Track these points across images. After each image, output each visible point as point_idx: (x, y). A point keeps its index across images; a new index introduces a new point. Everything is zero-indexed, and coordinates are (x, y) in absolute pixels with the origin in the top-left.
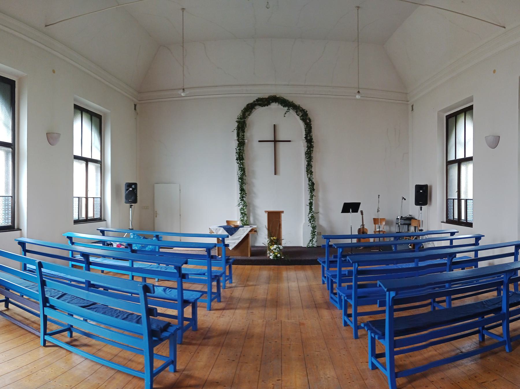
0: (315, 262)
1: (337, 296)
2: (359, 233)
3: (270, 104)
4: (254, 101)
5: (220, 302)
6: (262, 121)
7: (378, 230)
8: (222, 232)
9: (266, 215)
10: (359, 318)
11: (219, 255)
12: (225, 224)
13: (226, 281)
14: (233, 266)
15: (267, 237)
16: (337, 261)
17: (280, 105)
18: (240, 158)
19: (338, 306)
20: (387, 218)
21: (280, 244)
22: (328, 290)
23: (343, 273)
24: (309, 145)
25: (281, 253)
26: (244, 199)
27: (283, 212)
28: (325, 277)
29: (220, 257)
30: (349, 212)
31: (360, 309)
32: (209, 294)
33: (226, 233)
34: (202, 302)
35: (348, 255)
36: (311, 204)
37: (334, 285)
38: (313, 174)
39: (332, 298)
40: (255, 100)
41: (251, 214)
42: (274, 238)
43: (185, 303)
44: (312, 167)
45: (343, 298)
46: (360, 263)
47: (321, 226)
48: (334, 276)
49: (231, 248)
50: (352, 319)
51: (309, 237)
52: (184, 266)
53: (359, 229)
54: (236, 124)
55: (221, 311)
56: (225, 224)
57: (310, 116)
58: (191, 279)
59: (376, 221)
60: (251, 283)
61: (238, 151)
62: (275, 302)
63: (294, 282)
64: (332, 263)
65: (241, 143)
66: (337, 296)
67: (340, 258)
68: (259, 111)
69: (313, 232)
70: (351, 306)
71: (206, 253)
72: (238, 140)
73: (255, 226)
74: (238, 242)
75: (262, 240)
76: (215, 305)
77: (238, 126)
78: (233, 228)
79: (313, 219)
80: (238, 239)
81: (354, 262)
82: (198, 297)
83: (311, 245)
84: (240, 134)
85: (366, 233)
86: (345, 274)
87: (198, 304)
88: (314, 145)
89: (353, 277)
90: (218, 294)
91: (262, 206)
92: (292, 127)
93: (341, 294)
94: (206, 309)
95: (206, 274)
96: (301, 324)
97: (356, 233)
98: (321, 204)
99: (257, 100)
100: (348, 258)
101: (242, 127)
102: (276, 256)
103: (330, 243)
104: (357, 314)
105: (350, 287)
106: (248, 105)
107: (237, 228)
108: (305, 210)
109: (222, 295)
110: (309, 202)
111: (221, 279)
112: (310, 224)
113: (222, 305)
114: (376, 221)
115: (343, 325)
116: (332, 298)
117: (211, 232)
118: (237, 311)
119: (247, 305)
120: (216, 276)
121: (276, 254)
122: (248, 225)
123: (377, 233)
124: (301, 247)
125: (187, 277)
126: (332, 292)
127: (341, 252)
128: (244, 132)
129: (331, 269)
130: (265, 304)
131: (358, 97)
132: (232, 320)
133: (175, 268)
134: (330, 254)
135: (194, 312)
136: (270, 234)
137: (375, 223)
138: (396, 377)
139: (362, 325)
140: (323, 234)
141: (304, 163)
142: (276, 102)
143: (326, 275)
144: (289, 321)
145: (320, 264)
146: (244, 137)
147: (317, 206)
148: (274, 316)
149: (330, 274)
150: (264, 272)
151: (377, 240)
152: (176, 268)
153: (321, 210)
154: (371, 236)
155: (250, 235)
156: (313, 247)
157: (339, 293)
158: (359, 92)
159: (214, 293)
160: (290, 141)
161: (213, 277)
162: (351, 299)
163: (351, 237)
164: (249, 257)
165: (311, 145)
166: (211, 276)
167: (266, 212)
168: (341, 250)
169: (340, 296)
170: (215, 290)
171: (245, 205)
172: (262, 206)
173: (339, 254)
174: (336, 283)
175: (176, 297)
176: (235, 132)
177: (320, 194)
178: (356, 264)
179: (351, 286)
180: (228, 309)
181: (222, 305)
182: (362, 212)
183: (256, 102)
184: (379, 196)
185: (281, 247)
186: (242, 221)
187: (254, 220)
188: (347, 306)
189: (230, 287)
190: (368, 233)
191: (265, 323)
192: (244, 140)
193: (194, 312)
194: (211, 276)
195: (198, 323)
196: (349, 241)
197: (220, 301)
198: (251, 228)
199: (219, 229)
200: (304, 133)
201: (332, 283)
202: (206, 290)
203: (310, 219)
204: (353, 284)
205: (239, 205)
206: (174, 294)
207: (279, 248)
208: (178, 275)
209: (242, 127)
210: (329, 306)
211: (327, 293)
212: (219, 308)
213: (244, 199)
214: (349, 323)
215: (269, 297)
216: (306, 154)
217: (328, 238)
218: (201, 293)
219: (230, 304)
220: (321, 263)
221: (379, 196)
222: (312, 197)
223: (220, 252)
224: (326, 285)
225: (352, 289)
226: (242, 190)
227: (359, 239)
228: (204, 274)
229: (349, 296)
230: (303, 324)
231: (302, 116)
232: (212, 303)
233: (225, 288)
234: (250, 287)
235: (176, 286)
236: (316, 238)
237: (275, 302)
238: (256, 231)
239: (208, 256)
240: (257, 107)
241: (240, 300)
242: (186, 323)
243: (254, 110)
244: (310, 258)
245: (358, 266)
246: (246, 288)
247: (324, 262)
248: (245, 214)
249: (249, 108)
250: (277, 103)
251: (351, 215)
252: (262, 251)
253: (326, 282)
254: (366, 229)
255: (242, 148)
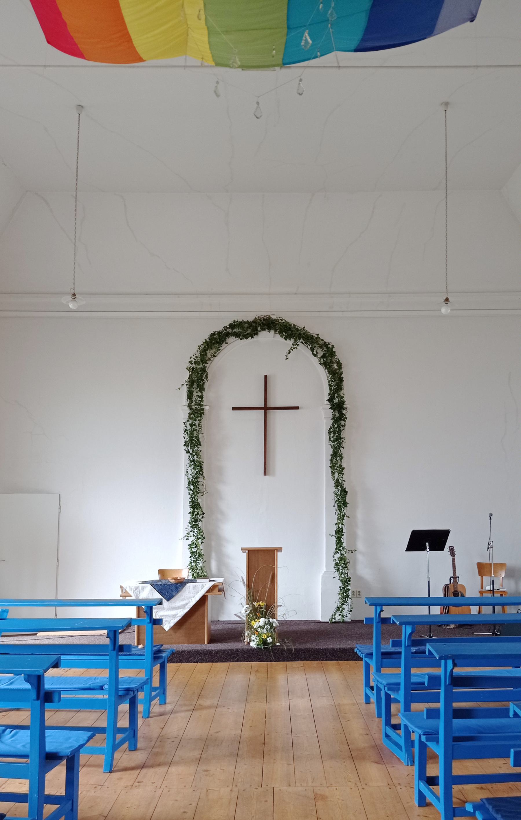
0: (348, 655)
1: (402, 732)
2: (445, 595)
3: (256, 334)
4: (226, 328)
5: (136, 749)
6: (239, 369)
7: (488, 588)
8: (150, 594)
9: (244, 556)
10: (456, 788)
11: (138, 644)
12: (156, 577)
13: (152, 699)
14: (170, 667)
15: (244, 601)
16: (400, 653)
17: (278, 336)
18: (193, 442)
19: (403, 755)
20: (510, 562)
21: (273, 616)
22: (380, 716)
23: (414, 680)
24: (338, 415)
25: (275, 635)
26: (200, 524)
27: (280, 549)
28: (372, 688)
29: (140, 646)
30: (423, 549)
31: (460, 768)
32: (110, 731)
33: (157, 596)
34: (93, 752)
35: (430, 641)
36: (339, 533)
37: (394, 707)
38: (345, 471)
39: (387, 736)
40: (227, 324)
41: (213, 555)
42: (261, 603)
43: (51, 759)
44: (342, 458)
45: (415, 737)
46: (457, 660)
47: (360, 579)
48: (394, 687)
49: (167, 626)
50: (440, 789)
51: (335, 600)
52: (52, 672)
53: (447, 585)
54: (187, 374)
55: (136, 772)
56: (156, 577)
57: (340, 355)
58: (67, 700)
59: (483, 569)
60: (207, 702)
61: (189, 427)
62: (260, 746)
63: (303, 697)
64: (388, 657)
65: (196, 413)
66: (402, 732)
67: (407, 647)
68: (234, 346)
69: (344, 594)
70: (435, 757)
71: (107, 641)
72: (190, 407)
73: (220, 580)
74: (181, 613)
75: (235, 608)
76: (124, 757)
77: (190, 377)
78: (172, 584)
79: (342, 564)
80: (184, 606)
81: (446, 658)
82: (82, 742)
83: (338, 618)
84: (195, 394)
85: (463, 595)
86: (423, 684)
87: (83, 758)
88: (348, 413)
89: (442, 691)
90: (132, 730)
91: (237, 538)
92: (302, 378)
93: (411, 727)
94: (102, 770)
95: (106, 687)
96: (317, 797)
97: (438, 593)
98: (360, 533)
99: (231, 325)
100: (428, 647)
101: (197, 379)
102: (265, 642)
103: (383, 615)
104: (452, 780)
105: (433, 714)
106: (213, 335)
107: (181, 584)
108: (326, 545)
109: (140, 734)
110: (335, 528)
111: (141, 696)
112: (337, 574)
113: (139, 757)
114: (483, 569)
115: (416, 803)
116: (387, 736)
117: (125, 593)
118: (173, 769)
119: (197, 753)
120: (128, 690)
121: (264, 637)
122: (205, 577)
123: (485, 595)
124: (319, 622)
125: (56, 697)
126: (388, 722)
127: (410, 634)
128: (202, 389)
129: (384, 671)
130: (237, 750)
131: (445, 310)
132: (159, 792)
133: (27, 681)
134: (383, 636)
135: (71, 782)
136: (252, 595)
137: (481, 574)
138: (454, 817)
139: (469, 808)
140: (364, 595)
141: (325, 450)
142: (269, 329)
143: (372, 684)
144: (290, 789)
145: (361, 659)
146: (202, 401)
147: (354, 537)
148: (258, 779)
149: (385, 683)
150: (237, 677)
151: (487, 610)
152: (28, 679)
153: (360, 546)
154: (474, 602)
155: (209, 598)
156: (343, 621)
157: (406, 727)
158: (447, 300)
159: (121, 730)
160: (297, 408)
161: (120, 693)
162: (438, 742)
163: (429, 602)
164: (207, 646)
165: (342, 414)
166: (117, 690)
167: (243, 549)
168: (409, 630)
169: (408, 733)
170: (124, 722)
171: (201, 536)
172: (237, 538)
173: (404, 639)
174: (398, 702)
175: (27, 750)
176: (185, 389)
177: (358, 511)
178: (450, 662)
179: (437, 711)
180: (151, 766)
181: (139, 757)
182: (452, 550)
183: (229, 330)
184: (491, 515)
185: (275, 622)
186: (192, 569)
187: (219, 569)
188: (426, 757)
189: (161, 714)
190: (467, 595)
191: (234, 795)
192: (201, 405)
193: (71, 782)
194: (117, 690)
195: (79, 808)
196: (423, 610)
197: (134, 748)
198: (212, 584)
199: (143, 588)
200: (326, 390)
201: (389, 700)
202: (103, 723)
203: (337, 564)
204: (440, 705)
205: (187, 536)
206: (22, 741)
207: (271, 625)
208: (34, 695)
209: (197, 379)
210: (381, 757)
211: (378, 725)
212: (133, 764)
213: (200, 524)
214: (430, 798)
215: (247, 733)
216: (330, 432)
217: (378, 603)
218: (89, 734)
219: (157, 754)
220: (362, 656)
221: (491, 515)
222: (341, 518)
223: (141, 638)
224: (373, 706)
225: (438, 717)
226: (195, 506)
227: (446, 608)
228: (101, 688)
229: (432, 735)
230: (323, 798)
231: (323, 356)
232: (117, 755)
233: (148, 715)
234: (205, 712)
235: (28, 723)
236: (349, 602)
237: (260, 746)
238: (221, 590)
239: (111, 648)
240: (231, 339)
241: (180, 742)
242: (49, 809)
243: (224, 345)
244: (337, 646)
245: (455, 665)
246: (196, 714)
247: (370, 655)
248: (200, 555)
249: (216, 341)
250: (272, 332)
251: (427, 556)
252: (234, 633)
253: (373, 699)
254: (463, 586)
255: (197, 422)
